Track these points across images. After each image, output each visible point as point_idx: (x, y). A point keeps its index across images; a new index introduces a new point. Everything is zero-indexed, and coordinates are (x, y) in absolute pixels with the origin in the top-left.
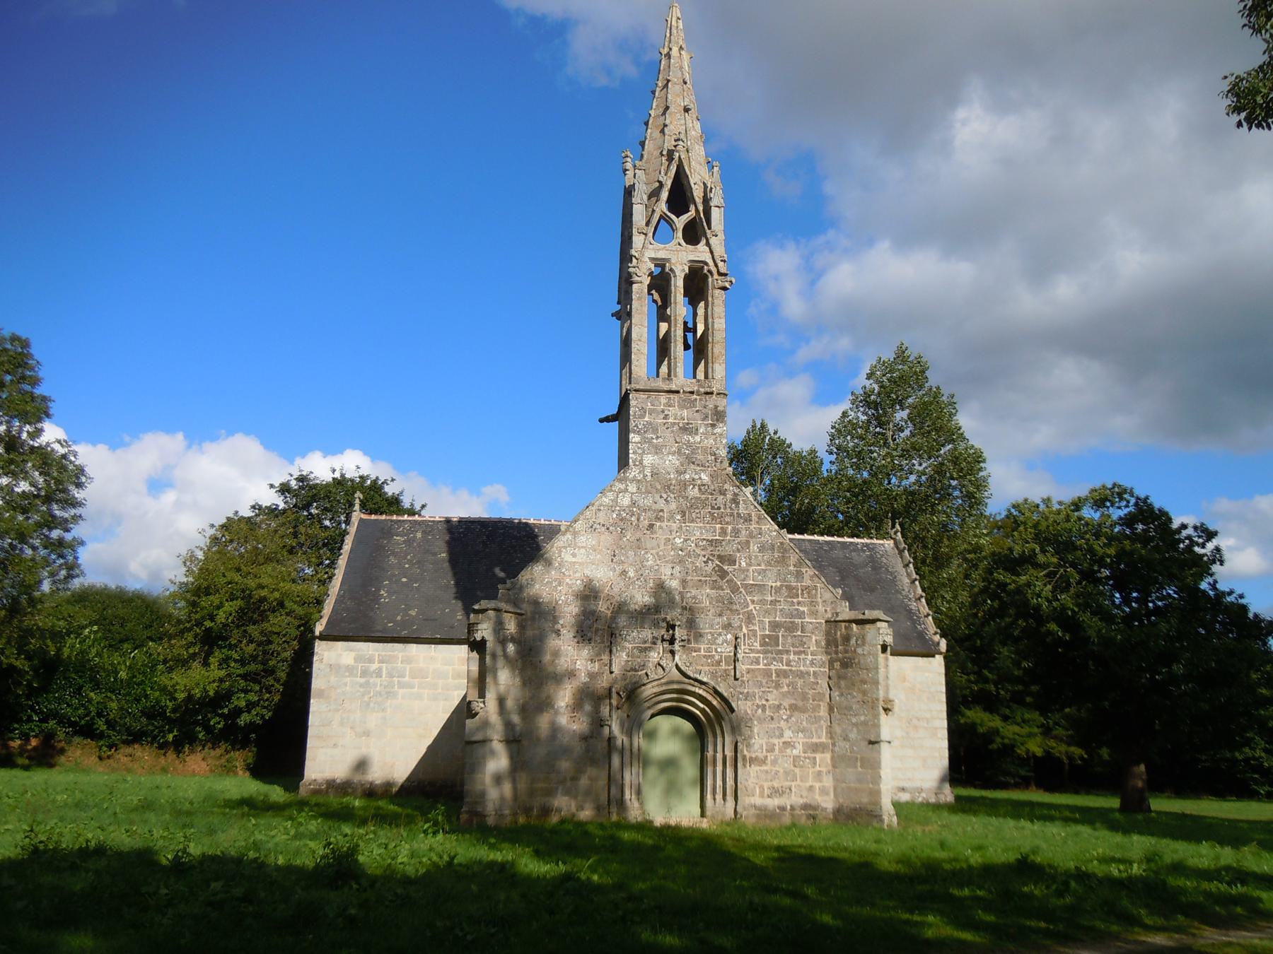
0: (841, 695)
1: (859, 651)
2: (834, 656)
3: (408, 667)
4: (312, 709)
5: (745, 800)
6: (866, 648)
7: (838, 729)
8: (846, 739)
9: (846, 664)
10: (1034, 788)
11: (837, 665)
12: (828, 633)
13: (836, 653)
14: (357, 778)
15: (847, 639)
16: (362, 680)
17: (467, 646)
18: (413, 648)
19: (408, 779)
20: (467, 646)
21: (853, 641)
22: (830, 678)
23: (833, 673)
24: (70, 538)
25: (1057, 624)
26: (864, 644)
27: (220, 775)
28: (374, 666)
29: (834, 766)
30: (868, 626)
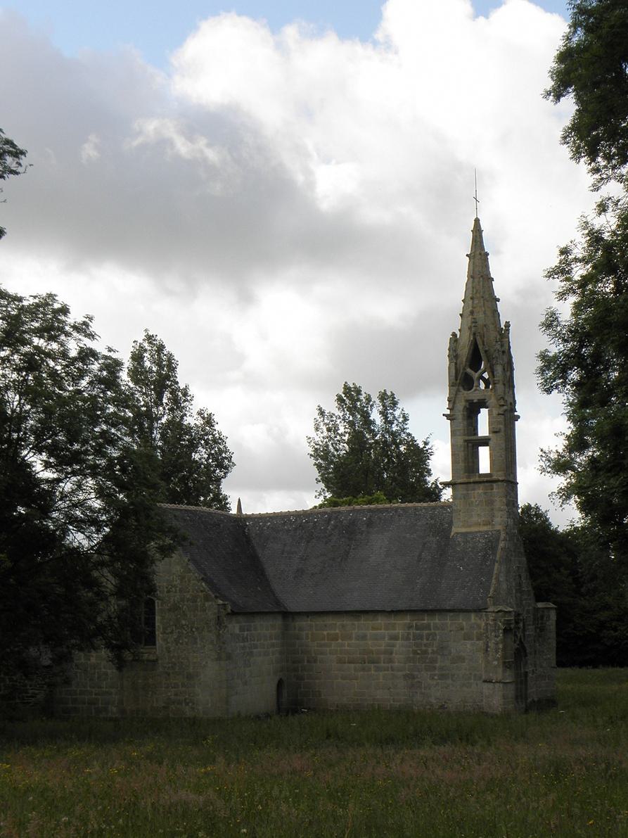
6: (551, 621)
11: (538, 630)
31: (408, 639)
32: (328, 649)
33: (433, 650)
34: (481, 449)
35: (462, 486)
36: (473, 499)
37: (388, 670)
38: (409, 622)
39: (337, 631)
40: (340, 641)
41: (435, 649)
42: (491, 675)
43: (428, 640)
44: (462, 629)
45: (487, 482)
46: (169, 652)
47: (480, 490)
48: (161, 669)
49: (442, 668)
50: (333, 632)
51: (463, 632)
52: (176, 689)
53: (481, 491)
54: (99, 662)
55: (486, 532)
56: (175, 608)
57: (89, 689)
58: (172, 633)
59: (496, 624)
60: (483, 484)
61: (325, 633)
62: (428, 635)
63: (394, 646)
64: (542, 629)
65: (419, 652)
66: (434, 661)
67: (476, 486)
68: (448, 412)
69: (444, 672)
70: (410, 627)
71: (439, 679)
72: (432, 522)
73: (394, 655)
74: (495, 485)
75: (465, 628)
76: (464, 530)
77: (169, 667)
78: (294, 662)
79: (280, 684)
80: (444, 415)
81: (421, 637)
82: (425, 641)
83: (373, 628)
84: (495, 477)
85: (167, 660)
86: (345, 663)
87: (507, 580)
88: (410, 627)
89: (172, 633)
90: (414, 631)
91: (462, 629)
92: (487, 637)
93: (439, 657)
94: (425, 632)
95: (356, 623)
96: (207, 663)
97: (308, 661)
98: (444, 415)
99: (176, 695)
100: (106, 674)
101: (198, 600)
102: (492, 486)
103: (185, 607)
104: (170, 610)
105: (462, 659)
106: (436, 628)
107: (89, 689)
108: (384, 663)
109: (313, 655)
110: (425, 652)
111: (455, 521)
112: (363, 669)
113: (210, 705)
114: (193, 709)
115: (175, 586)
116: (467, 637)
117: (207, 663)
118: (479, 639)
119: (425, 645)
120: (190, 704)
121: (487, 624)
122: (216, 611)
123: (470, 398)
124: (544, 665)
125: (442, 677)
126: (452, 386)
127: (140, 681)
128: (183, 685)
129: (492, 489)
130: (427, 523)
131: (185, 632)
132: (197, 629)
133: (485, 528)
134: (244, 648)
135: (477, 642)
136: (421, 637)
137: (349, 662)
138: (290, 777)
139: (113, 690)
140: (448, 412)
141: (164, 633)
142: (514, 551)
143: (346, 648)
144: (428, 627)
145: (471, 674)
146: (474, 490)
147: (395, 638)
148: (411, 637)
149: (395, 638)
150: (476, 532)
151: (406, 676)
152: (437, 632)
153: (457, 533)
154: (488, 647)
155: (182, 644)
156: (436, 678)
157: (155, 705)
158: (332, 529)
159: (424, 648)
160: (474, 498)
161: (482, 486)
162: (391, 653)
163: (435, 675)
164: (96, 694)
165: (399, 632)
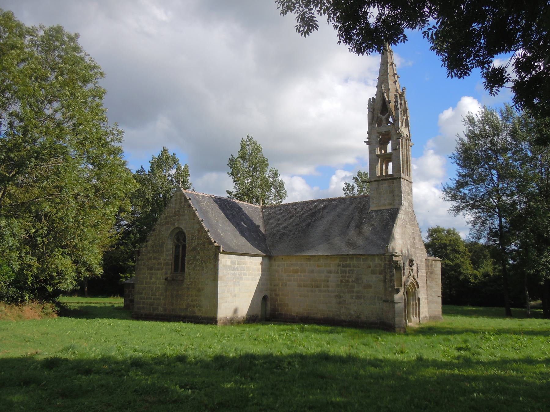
0: (430, 282)
1: (435, 269)
2: (428, 270)
3: (245, 266)
4: (219, 285)
5: (422, 316)
6: (437, 268)
7: (429, 293)
8: (431, 296)
9: (431, 273)
10: (119, 297)
11: (429, 273)
12: (426, 263)
13: (428, 269)
14: (235, 316)
15: (432, 265)
16: (233, 272)
17: (261, 258)
18: (247, 258)
19: (247, 315)
20: (261, 258)
21: (433, 266)
22: (426, 277)
23: (427, 276)
24: (468, 216)
25: (393, 259)
26: (436, 267)
27: (252, 323)
28: (236, 266)
29: (428, 304)
30: (437, 262)
31: (338, 273)
32: (293, 278)
33: (352, 280)
34: (389, 163)
35: (375, 182)
36: (381, 190)
37: (326, 292)
38: (338, 262)
39: (298, 268)
40: (299, 273)
41: (354, 280)
42: (388, 297)
43: (349, 273)
44: (370, 267)
45: (390, 179)
46: (190, 275)
47: (386, 185)
48: (185, 286)
49: (357, 292)
50: (296, 268)
51: (370, 269)
52: (192, 298)
53: (386, 185)
54: (156, 280)
55: (390, 210)
56: (194, 249)
57: (150, 296)
58: (192, 264)
59: (390, 263)
60: (388, 181)
61: (291, 268)
62: (350, 271)
63: (329, 277)
64: (431, 273)
65: (344, 281)
66: (353, 287)
67: (384, 182)
68: (367, 140)
69: (359, 294)
70: (339, 265)
71: (356, 299)
72: (359, 205)
73: (329, 282)
74: (395, 181)
75: (372, 266)
76: (376, 209)
77: (189, 284)
78: (274, 286)
79: (265, 298)
80: (365, 142)
81: (345, 272)
82: (347, 274)
83: (318, 266)
84: (395, 176)
85: (189, 280)
86: (302, 287)
87: (403, 239)
88: (339, 265)
89: (192, 264)
90: (341, 268)
91: (370, 267)
92: (385, 272)
93: (356, 284)
94: (348, 269)
95: (308, 263)
96: (208, 282)
97: (282, 285)
98: (365, 142)
99: (192, 301)
100: (159, 288)
101: (206, 244)
102: (393, 181)
103: (199, 248)
104: (192, 250)
105: (369, 286)
106: (354, 266)
107: (150, 296)
108: (324, 287)
109: (285, 282)
110: (348, 281)
111: (371, 203)
112: (312, 291)
113: (208, 308)
114: (200, 310)
115: (195, 236)
116: (373, 272)
117: (208, 282)
118: (380, 274)
119: (348, 277)
120: (199, 307)
121: (385, 264)
122: (214, 251)
123: (380, 131)
124: (433, 295)
125: (358, 297)
126: (370, 125)
127: (175, 292)
128: (196, 296)
129: (393, 184)
130: (356, 206)
131: (198, 263)
132: (204, 261)
133: (389, 207)
134: (234, 274)
135: (380, 276)
136: (345, 272)
137: (304, 286)
138: (510, 346)
139: (162, 297)
140: (367, 140)
141: (188, 264)
142: (409, 222)
143: (303, 278)
144: (349, 266)
145: (375, 296)
146: (382, 184)
147: (330, 272)
148: (339, 271)
149: (330, 272)
150: (383, 210)
151: (336, 296)
152: (355, 269)
153: (372, 211)
154: (385, 278)
155: (196, 270)
156: (354, 298)
157: (181, 307)
158: (304, 211)
159: (347, 279)
160: (382, 189)
161: (387, 182)
162: (328, 282)
163: (353, 296)
164: (154, 299)
165: (333, 268)
